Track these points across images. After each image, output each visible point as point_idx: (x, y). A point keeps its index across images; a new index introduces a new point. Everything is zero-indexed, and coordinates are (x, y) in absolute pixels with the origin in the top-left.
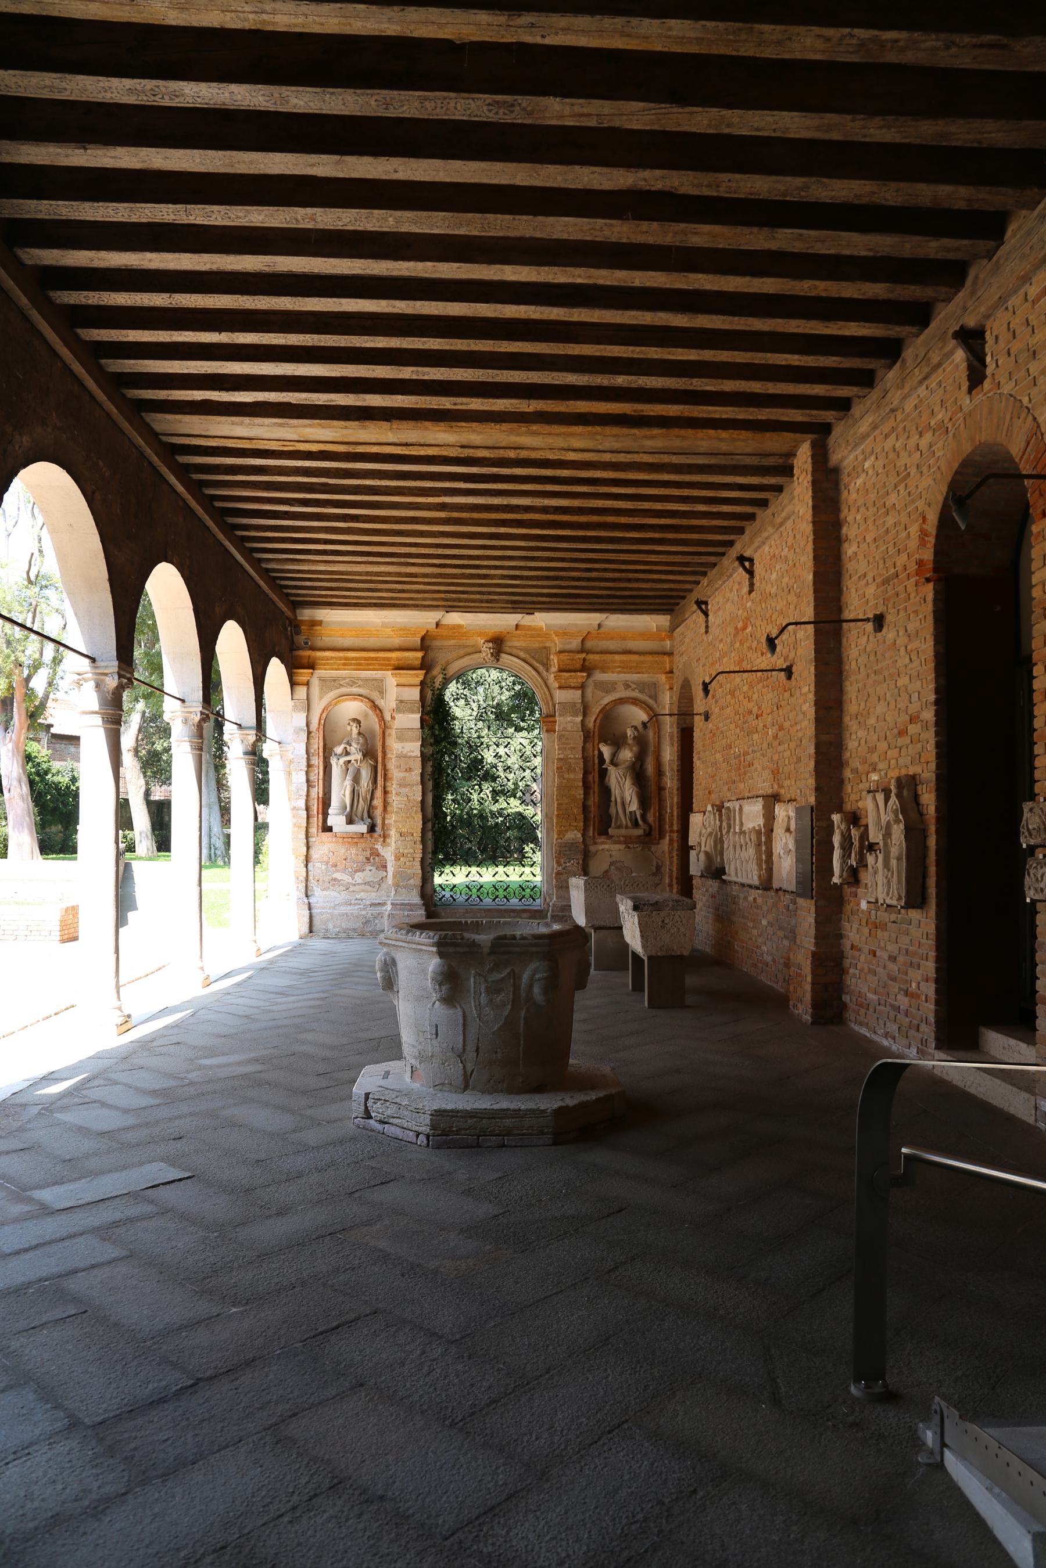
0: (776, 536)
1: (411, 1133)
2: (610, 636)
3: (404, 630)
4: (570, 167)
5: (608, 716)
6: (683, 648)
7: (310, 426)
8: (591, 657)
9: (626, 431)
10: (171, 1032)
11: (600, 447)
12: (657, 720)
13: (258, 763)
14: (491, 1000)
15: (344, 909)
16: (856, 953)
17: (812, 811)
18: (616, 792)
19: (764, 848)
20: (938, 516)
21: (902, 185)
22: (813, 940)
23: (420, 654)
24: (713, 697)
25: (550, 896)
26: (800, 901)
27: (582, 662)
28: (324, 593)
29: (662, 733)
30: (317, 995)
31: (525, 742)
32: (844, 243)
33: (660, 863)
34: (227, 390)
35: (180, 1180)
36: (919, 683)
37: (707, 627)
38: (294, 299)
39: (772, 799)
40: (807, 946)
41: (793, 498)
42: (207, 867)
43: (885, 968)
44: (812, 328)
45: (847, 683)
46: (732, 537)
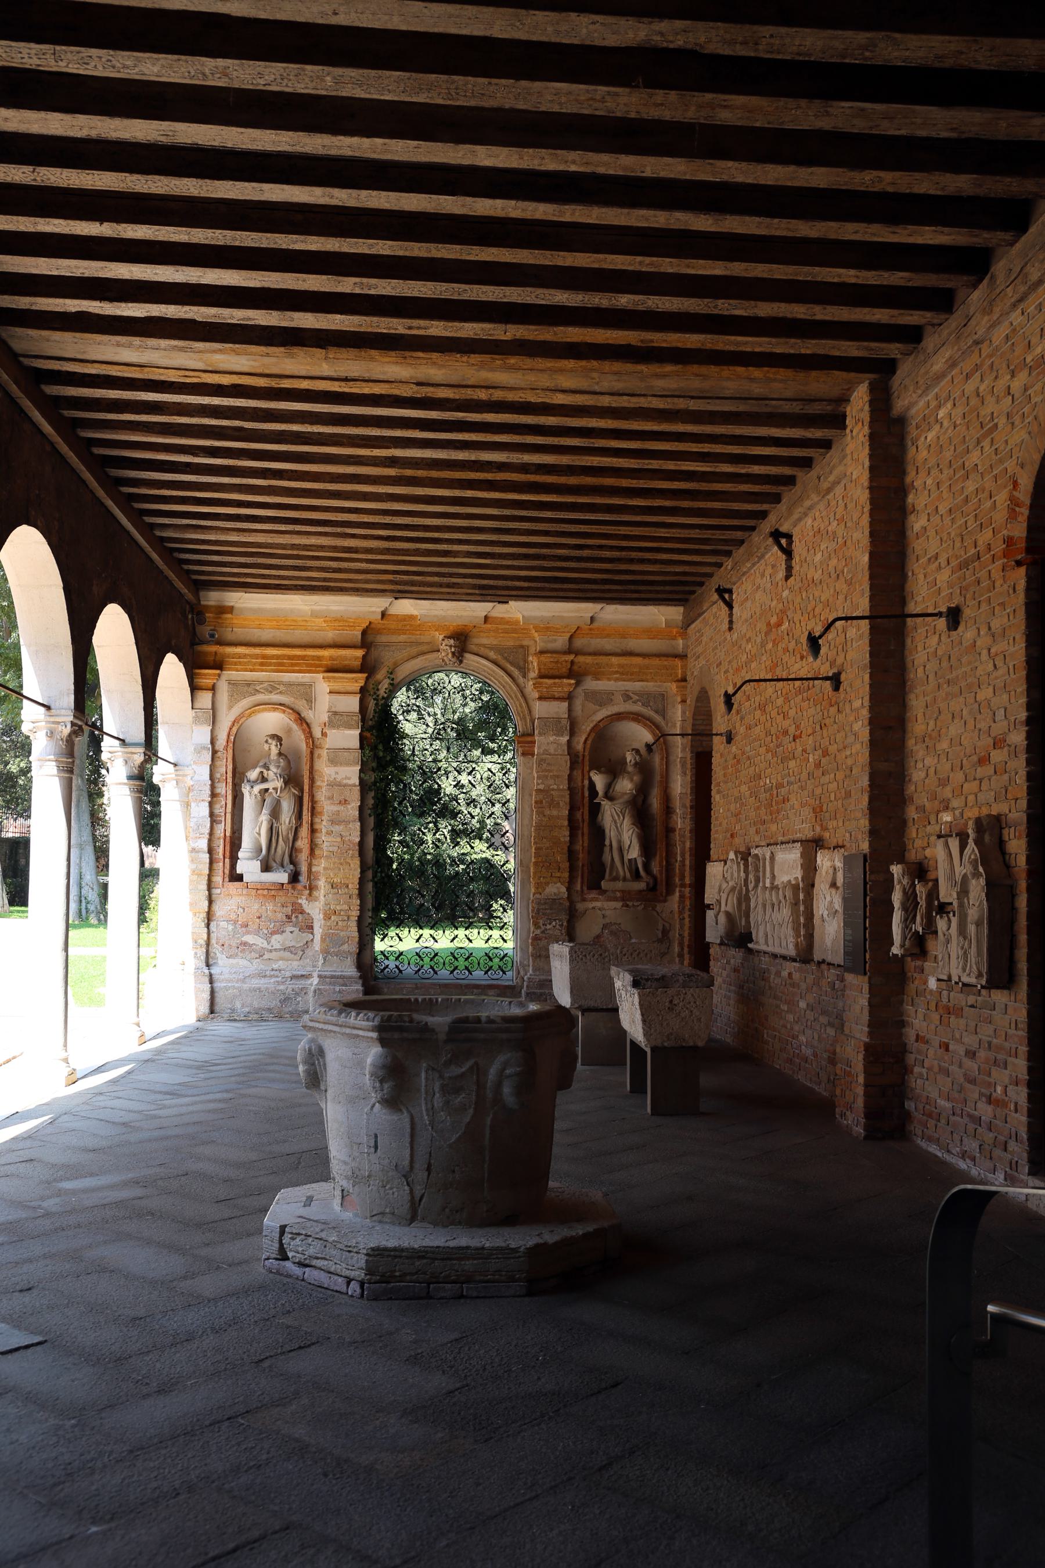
0: (821, 506)
1: (340, 1280)
2: (605, 632)
3: (340, 621)
4: (564, 14)
5: (601, 735)
6: (700, 649)
7: (220, 351)
8: (581, 659)
9: (630, 367)
10: (21, 1145)
11: (597, 388)
12: (665, 742)
13: (147, 795)
14: (447, 1103)
15: (256, 983)
16: (923, 1047)
17: (865, 860)
18: (611, 833)
19: (802, 908)
20: (1034, 479)
21: (998, 41)
22: (866, 1029)
23: (360, 653)
24: (738, 712)
25: (525, 967)
26: (850, 977)
27: (570, 666)
28: (235, 570)
29: (672, 758)
30: (219, 1096)
31: (495, 768)
32: (919, 121)
33: (667, 925)
34: (111, 300)
35: (27, 1347)
36: (1005, 697)
37: (731, 622)
38: (200, 182)
39: (813, 845)
40: (858, 1036)
41: (845, 457)
42: (75, 927)
43: (960, 1066)
44: (874, 235)
45: (912, 696)
46: (765, 507)
